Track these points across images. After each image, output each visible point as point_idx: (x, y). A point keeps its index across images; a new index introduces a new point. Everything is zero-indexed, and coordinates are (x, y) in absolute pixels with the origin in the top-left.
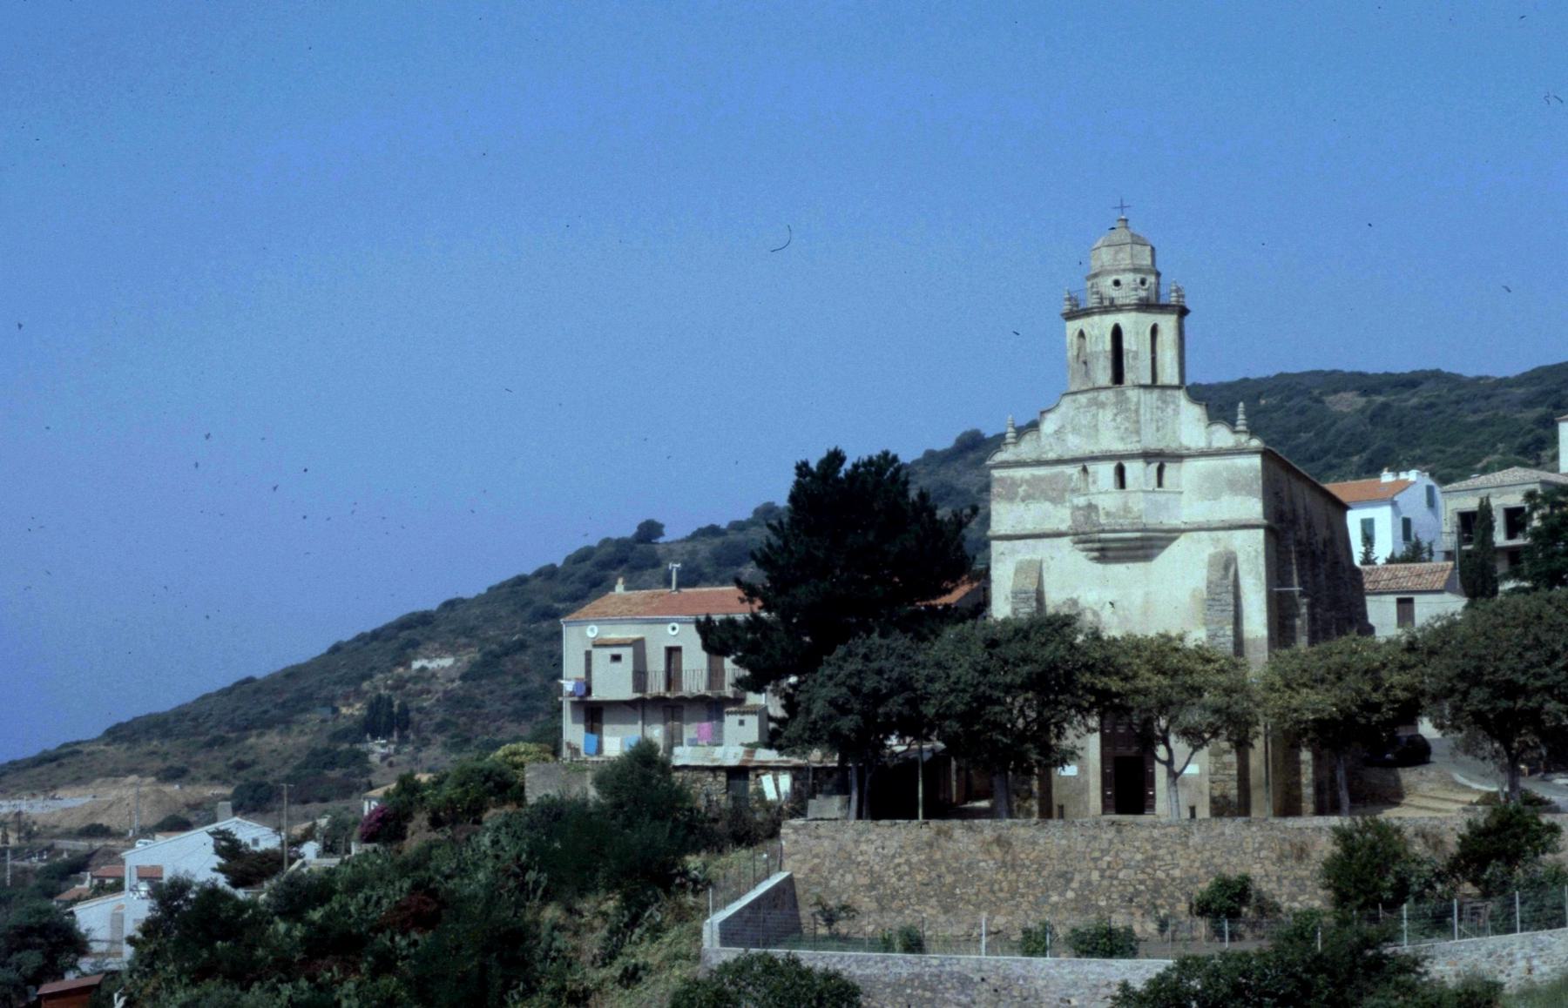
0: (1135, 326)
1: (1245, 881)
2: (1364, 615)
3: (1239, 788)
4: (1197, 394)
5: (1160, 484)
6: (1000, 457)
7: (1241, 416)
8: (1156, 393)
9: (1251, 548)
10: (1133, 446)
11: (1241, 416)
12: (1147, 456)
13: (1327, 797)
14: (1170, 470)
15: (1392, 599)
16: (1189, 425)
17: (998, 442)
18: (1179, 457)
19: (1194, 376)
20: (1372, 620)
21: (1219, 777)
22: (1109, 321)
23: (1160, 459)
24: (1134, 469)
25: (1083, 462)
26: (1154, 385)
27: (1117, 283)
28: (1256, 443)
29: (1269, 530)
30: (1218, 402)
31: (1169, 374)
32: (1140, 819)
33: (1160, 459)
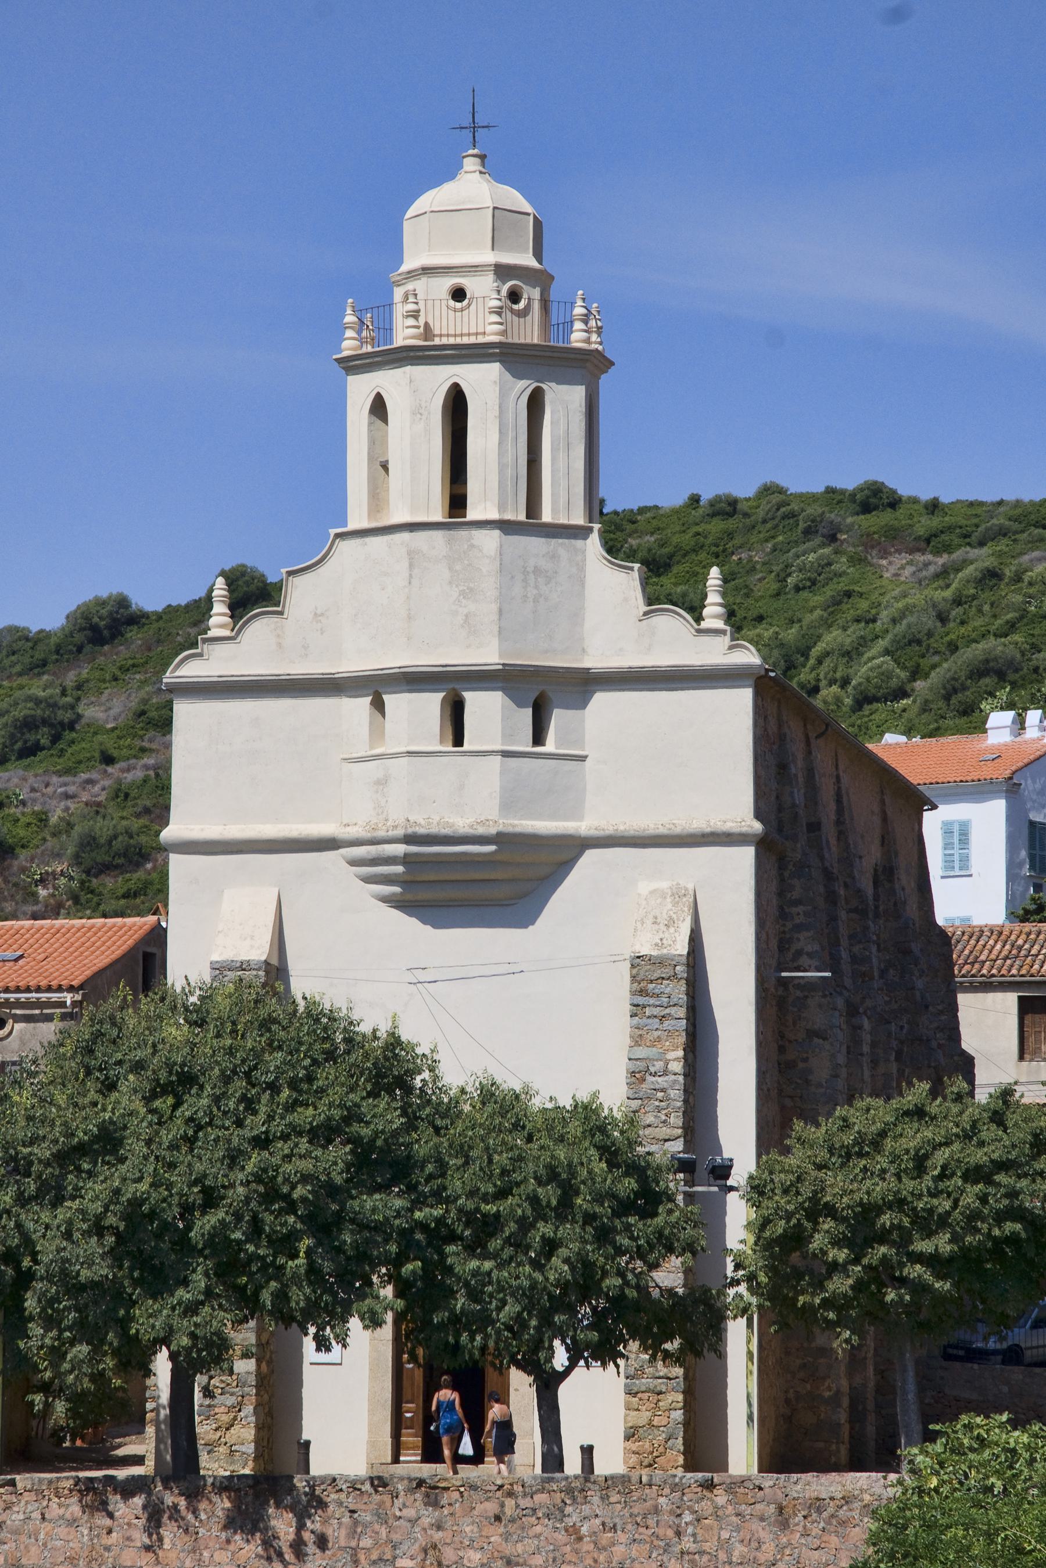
0: (483, 382)
1: (936, 499)
2: (955, 1035)
3: (257, 1441)
4: (621, 534)
5: (538, 738)
6: (190, 670)
7: (713, 598)
8: (535, 544)
9: (728, 893)
10: (488, 655)
11: (713, 598)
12: (506, 679)
13: (871, 1430)
14: (558, 719)
15: (1010, 1000)
16: (608, 613)
17: (185, 626)
18: (583, 684)
19: (619, 498)
20: (968, 1043)
21: (644, 1383)
22: (437, 379)
23: (543, 693)
24: (485, 708)
25: (376, 687)
26: (530, 524)
27: (459, 294)
28: (749, 657)
29: (764, 846)
30: (663, 554)
31: (562, 500)
32: (330, 1539)
33: (543, 693)
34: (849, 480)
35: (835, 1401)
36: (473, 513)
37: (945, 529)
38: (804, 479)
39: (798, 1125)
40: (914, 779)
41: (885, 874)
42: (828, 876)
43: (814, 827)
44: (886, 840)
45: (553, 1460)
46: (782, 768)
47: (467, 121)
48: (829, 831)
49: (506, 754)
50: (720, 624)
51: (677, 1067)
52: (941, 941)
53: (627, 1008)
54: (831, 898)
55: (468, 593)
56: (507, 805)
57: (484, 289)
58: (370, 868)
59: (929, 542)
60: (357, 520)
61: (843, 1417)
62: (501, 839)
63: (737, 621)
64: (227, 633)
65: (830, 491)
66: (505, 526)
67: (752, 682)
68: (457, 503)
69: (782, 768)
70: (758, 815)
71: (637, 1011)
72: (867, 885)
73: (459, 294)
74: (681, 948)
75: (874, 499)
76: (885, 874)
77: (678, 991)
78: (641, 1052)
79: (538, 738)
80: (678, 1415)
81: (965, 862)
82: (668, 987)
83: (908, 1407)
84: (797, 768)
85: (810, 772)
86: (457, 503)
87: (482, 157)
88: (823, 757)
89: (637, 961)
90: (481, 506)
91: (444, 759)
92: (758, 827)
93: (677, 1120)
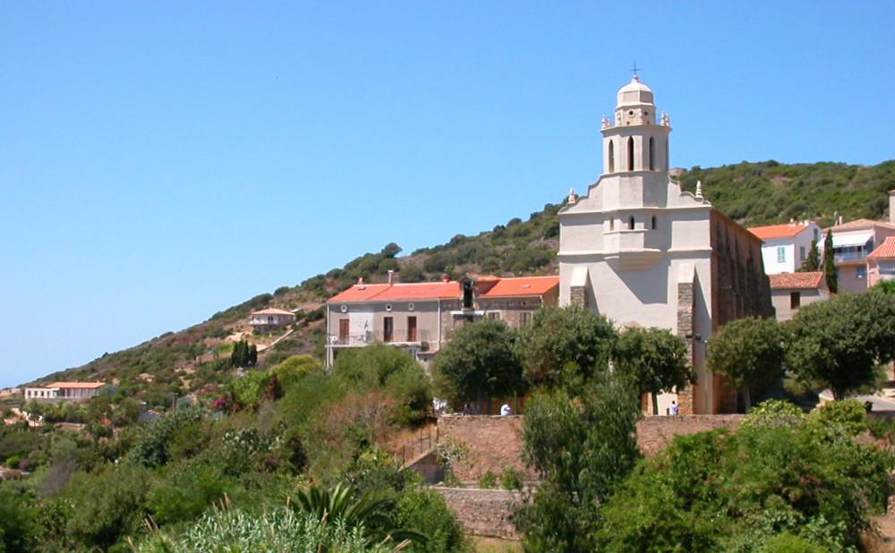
9: (705, 268)
25: (611, 216)
27: (631, 113)
34: (765, 159)
35: (733, 396)
36: (635, 169)
37: (790, 172)
38: (753, 160)
39: (221, 412)
40: (760, 237)
41: (750, 261)
42: (732, 261)
43: (728, 249)
44: (750, 252)
45: (656, 411)
46: (719, 234)
47: (633, 68)
48: (733, 250)
49: (621, 233)
50: (701, 197)
51: (690, 311)
52: (766, 278)
53: (677, 297)
54: (733, 267)
55: (634, 190)
56: (621, 246)
57: (638, 112)
58: (612, 263)
59: (785, 175)
60: (607, 172)
61: (735, 400)
62: (620, 254)
63: (706, 197)
64: (574, 202)
65: (760, 163)
66: (622, 175)
67: (708, 214)
68: (631, 167)
69: (719, 234)
70: (711, 246)
71: (680, 297)
72: (745, 265)
73: (631, 113)
74: (691, 281)
75: (773, 164)
76: (750, 261)
77: (690, 292)
78: (680, 308)
79: (633, 228)
80: (691, 400)
81: (783, 258)
82: (688, 291)
83: (747, 401)
84: (723, 233)
85: (727, 234)
86: (631, 167)
87: (636, 78)
88: (731, 231)
89: (679, 284)
90: (617, 169)
91: (629, 234)
92: (711, 248)
93: (690, 325)
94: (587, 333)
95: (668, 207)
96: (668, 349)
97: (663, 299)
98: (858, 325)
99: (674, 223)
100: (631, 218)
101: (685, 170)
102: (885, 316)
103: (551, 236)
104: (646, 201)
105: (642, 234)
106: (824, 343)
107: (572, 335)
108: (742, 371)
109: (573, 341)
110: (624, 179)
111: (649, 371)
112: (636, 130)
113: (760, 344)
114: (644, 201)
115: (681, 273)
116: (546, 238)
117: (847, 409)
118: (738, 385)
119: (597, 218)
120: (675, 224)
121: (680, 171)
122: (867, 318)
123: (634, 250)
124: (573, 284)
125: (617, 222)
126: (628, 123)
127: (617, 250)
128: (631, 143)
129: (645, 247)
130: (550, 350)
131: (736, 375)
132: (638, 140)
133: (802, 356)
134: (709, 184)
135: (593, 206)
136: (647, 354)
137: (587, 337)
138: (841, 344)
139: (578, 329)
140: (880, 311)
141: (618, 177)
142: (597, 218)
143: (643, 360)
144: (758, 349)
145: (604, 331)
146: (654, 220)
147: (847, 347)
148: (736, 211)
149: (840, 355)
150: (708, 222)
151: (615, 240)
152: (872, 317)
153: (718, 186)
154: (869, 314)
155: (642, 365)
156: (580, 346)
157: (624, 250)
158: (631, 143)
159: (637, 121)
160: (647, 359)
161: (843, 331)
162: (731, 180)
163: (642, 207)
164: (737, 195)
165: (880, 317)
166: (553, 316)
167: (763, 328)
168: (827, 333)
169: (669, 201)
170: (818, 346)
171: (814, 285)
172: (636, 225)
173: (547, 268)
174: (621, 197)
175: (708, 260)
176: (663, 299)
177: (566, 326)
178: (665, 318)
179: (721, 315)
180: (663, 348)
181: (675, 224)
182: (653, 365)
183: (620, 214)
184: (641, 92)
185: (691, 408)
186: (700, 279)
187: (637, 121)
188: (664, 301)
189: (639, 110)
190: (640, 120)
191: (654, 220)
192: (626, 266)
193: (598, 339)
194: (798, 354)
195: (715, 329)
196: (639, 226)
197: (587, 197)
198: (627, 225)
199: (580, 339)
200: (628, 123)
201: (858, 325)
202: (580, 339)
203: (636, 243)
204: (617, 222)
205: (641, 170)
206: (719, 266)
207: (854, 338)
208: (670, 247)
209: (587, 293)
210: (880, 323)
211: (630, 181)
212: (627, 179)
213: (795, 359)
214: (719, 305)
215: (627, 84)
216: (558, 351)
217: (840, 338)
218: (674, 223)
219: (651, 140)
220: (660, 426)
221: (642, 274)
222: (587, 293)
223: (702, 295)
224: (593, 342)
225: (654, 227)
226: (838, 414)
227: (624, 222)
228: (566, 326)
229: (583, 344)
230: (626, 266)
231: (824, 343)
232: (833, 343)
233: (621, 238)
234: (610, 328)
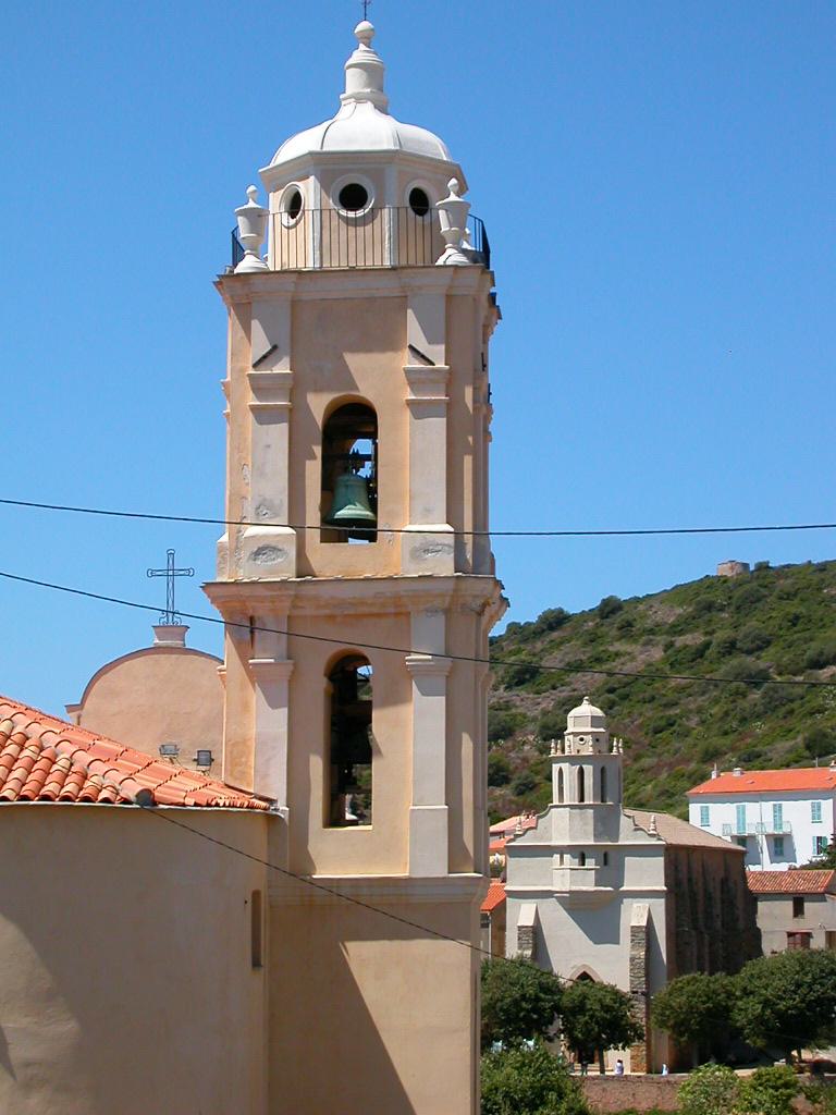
9: (659, 906)
25: (562, 850)
58: (561, 901)
67: (662, 852)
71: (633, 940)
74: (644, 924)
77: (642, 935)
79: (584, 865)
81: (819, 817)
86: (582, 800)
92: (665, 888)
94: (531, 991)
95: (619, 843)
96: (613, 1007)
97: (614, 939)
98: (799, 986)
99: (626, 859)
100: (581, 854)
101: (746, 566)
102: (827, 975)
103: (517, 684)
104: (597, 836)
105: (593, 872)
106: (766, 1003)
107: (516, 992)
108: (686, 1030)
109: (516, 999)
110: (574, 811)
111: (593, 1029)
112: (586, 759)
113: (704, 1003)
114: (595, 835)
115: (634, 914)
116: (509, 687)
117: (777, 1075)
118: (683, 1044)
119: (548, 851)
120: (627, 860)
121: (739, 569)
122: (808, 979)
123: (584, 888)
124: (519, 924)
125: (567, 857)
126: (578, 751)
127: (567, 888)
128: (581, 772)
129: (596, 885)
130: (494, 1008)
131: (682, 1035)
132: (588, 769)
133: (746, 1016)
134: (781, 598)
135: (541, 839)
136: (591, 1012)
137: (530, 995)
138: (782, 1006)
139: (522, 986)
140: (822, 971)
141: (568, 809)
142: (548, 851)
143: (587, 1018)
144: (702, 1007)
145: (550, 987)
146: (606, 855)
147: (789, 1009)
148: (821, 654)
149: (780, 1015)
150: (662, 859)
151: (564, 877)
152: (813, 977)
153: (796, 601)
154: (810, 975)
155: (586, 1023)
156: (524, 1005)
157: (574, 888)
158: (581, 772)
159: (588, 751)
160: (592, 1017)
161: (784, 992)
162: (820, 590)
163: (592, 843)
164: (826, 620)
165: (823, 977)
166: (498, 972)
167: (708, 986)
168: (768, 993)
169: (621, 836)
170: (760, 1006)
171: (821, 890)
172: (587, 860)
173: (510, 744)
174: (570, 830)
175: (663, 900)
176: (614, 939)
177: (511, 984)
178: (615, 967)
179: (679, 962)
180: (607, 1006)
181: (627, 860)
182: (597, 1023)
183: (571, 849)
184: (592, 717)
185: (644, 1060)
186: (654, 920)
187: (588, 751)
188: (616, 941)
189: (590, 737)
190: (591, 749)
191: (606, 855)
192: (576, 904)
193: (542, 995)
194: (743, 1013)
195: (669, 978)
196: (590, 863)
197: (535, 828)
198: (577, 860)
199: (523, 997)
200: (578, 751)
201: (799, 986)
202: (523, 997)
203: (587, 882)
204: (567, 857)
205: (592, 803)
206: (677, 903)
207: (794, 1000)
208: (622, 886)
209: (535, 934)
210: (822, 985)
211: (581, 814)
212: (578, 811)
213: (740, 1018)
214: (677, 946)
215: (576, 706)
216: (501, 1010)
217: (781, 998)
218: (626, 859)
219: (603, 770)
220: (605, 1086)
221: (594, 913)
222: (535, 934)
223: (657, 940)
224: (537, 999)
225: (606, 863)
226: (768, 1080)
227: (574, 857)
228: (511, 984)
229: (526, 1002)
230: (576, 904)
231: (766, 1003)
232: (775, 1004)
233: (571, 875)
234: (556, 983)
